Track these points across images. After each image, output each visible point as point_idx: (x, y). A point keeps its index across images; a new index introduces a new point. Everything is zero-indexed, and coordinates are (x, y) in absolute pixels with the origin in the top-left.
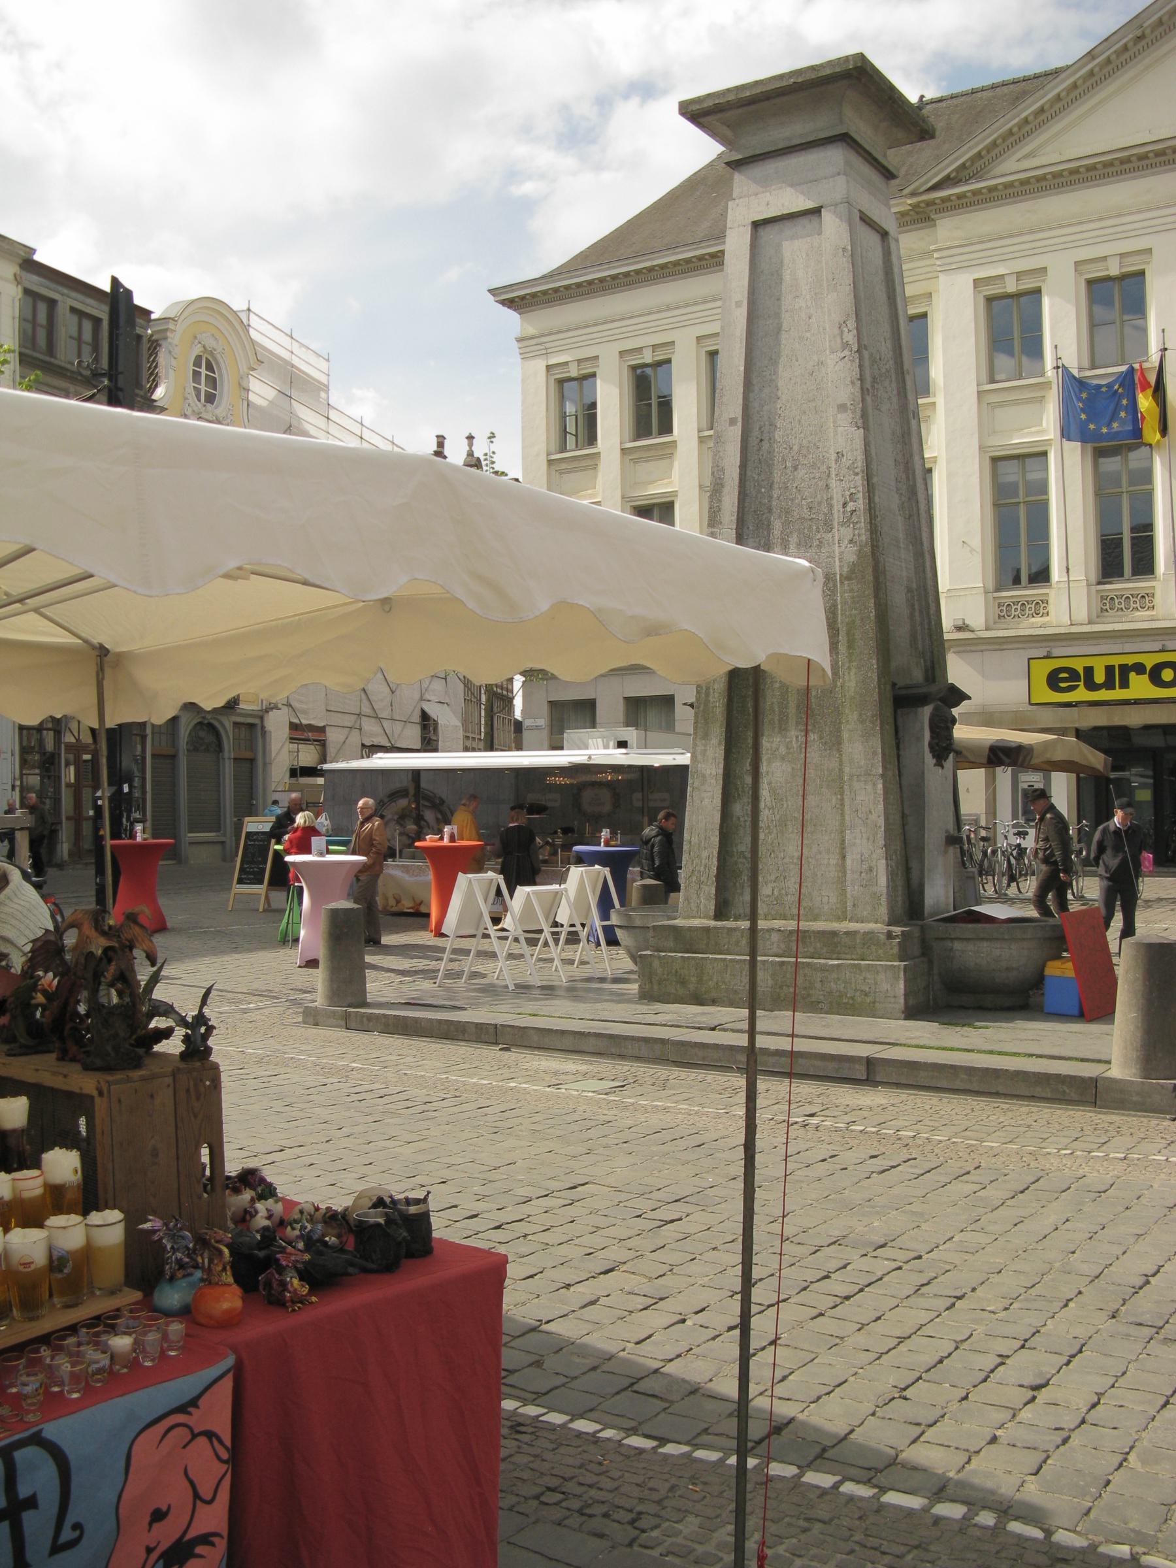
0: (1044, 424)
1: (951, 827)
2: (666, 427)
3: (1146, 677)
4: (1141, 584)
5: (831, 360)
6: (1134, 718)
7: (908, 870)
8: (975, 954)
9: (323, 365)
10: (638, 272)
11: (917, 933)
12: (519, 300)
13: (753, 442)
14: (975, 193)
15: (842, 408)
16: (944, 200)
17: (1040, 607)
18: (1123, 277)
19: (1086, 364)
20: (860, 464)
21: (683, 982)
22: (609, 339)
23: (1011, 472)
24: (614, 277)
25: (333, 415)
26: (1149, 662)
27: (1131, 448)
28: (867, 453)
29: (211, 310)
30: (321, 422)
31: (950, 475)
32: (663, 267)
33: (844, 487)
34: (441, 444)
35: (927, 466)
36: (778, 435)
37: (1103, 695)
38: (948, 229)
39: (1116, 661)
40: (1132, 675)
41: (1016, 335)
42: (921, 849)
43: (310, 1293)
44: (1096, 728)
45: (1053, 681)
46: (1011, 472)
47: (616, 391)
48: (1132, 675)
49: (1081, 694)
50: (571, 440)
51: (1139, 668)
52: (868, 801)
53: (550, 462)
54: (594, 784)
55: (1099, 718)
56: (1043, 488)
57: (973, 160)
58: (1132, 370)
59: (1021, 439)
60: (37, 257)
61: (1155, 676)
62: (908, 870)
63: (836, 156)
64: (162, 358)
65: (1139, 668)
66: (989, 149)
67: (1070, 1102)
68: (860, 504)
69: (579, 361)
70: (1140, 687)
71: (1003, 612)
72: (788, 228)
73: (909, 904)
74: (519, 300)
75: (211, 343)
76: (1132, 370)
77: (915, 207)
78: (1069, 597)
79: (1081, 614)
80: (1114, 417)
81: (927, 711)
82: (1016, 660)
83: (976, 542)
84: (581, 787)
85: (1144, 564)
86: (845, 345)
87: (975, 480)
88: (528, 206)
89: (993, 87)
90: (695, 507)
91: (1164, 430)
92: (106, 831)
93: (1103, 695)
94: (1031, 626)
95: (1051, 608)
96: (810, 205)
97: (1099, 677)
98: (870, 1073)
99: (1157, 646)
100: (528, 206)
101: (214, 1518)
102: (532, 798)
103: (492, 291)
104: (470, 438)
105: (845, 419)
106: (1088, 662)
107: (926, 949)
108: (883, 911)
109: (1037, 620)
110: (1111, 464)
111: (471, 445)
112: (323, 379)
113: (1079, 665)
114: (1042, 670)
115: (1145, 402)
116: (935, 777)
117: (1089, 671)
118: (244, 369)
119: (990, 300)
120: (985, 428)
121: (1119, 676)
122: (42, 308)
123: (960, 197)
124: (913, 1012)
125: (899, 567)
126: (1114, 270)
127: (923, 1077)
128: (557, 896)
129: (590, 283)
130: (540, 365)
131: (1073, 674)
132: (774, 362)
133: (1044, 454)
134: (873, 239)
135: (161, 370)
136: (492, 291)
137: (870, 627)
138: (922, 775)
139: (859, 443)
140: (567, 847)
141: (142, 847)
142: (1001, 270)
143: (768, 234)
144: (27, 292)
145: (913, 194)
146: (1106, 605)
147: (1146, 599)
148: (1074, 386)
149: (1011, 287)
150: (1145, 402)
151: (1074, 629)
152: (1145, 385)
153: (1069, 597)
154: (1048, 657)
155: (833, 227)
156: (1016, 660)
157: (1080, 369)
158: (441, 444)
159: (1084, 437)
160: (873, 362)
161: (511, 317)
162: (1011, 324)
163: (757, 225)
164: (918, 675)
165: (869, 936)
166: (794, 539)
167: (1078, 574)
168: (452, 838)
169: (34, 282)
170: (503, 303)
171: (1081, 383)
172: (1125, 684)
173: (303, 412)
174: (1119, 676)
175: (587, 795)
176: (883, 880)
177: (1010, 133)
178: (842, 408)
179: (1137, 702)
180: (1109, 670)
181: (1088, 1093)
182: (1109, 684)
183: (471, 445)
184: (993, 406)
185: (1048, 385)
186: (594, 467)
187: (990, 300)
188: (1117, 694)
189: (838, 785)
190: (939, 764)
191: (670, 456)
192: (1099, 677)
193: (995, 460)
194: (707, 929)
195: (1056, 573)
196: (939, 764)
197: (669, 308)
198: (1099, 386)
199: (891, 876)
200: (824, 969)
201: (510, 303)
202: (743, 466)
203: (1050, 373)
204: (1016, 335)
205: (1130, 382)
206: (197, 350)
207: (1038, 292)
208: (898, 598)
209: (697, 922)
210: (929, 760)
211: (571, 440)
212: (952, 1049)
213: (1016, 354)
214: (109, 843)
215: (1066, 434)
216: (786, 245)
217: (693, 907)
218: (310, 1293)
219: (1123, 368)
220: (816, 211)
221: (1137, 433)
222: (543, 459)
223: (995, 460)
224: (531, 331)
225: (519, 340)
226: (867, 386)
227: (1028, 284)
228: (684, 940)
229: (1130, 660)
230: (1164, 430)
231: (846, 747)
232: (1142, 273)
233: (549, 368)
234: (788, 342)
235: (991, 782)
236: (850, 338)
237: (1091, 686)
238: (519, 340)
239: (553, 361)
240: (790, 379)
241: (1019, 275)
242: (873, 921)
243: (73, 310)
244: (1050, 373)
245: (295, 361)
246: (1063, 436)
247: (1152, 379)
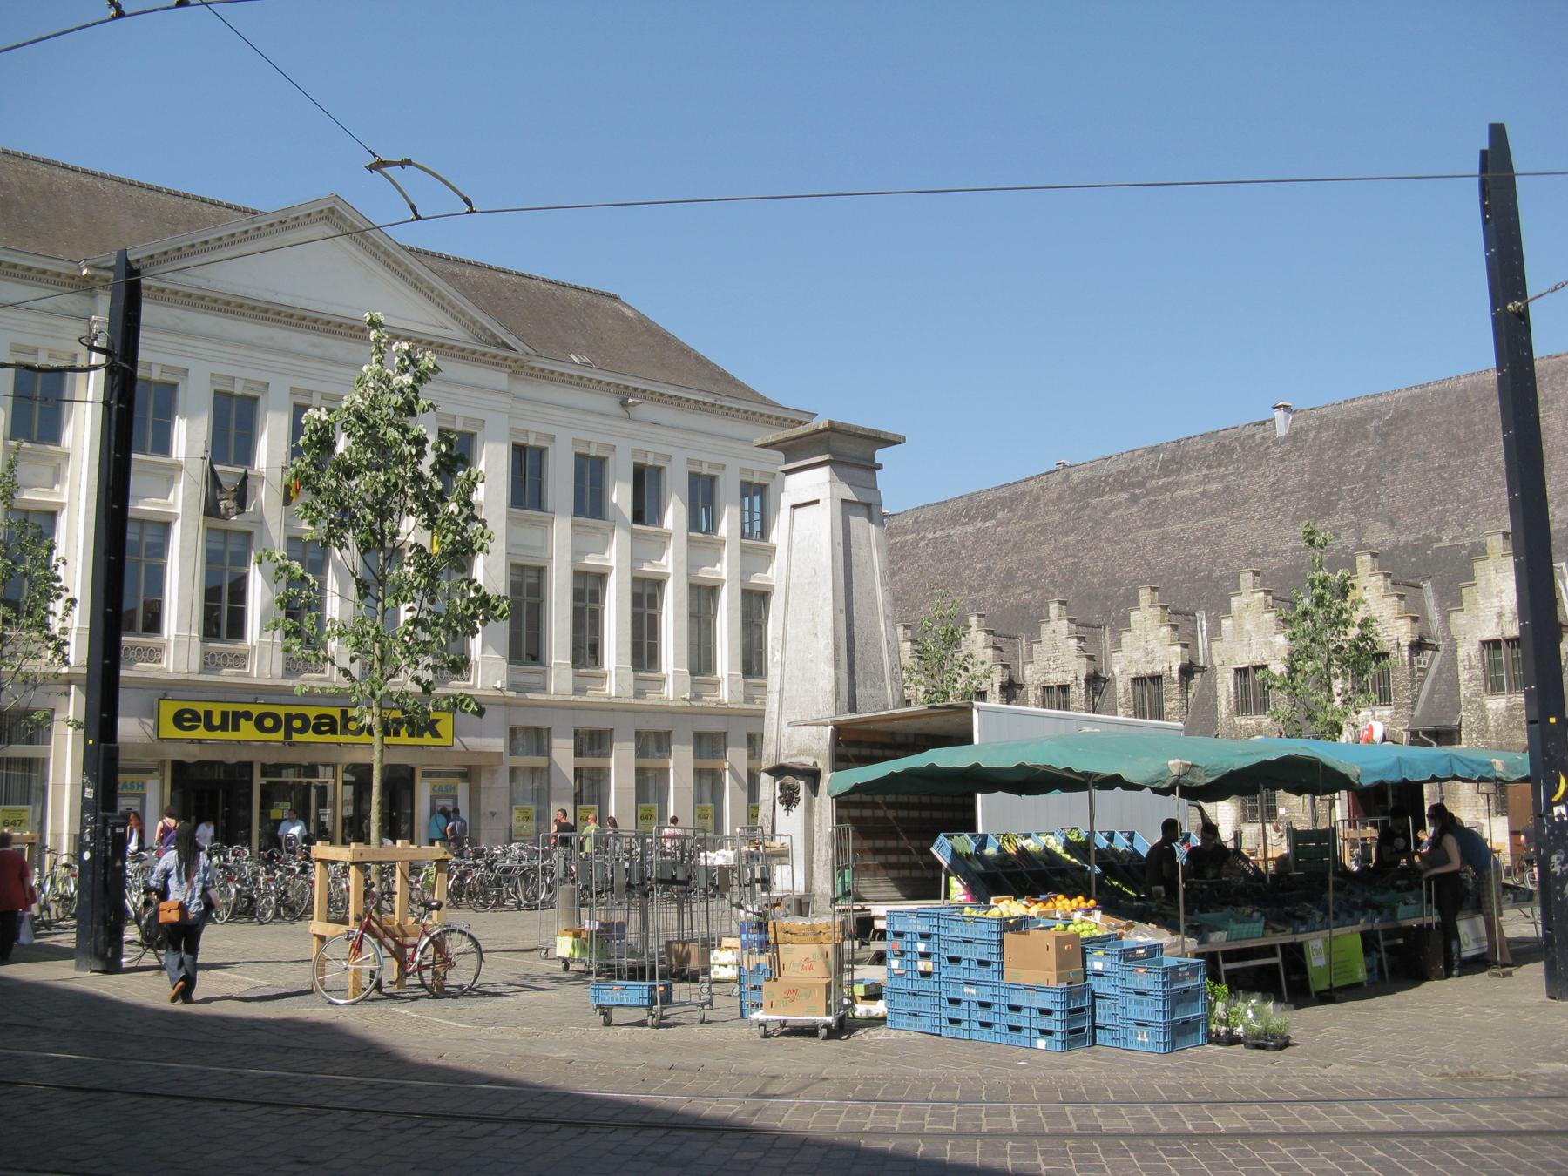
3: (252, 723)
18: (242, 398)
26: (256, 710)
39: (230, 708)
40: (242, 721)
43: (203, 849)
45: (179, 719)
48: (242, 721)
49: (201, 733)
61: (260, 726)
70: (247, 731)
97: (216, 720)
106: (208, 706)
113: (200, 708)
114: (169, 710)
117: (208, 714)
126: (238, 390)
131: (195, 716)
146: (211, 662)
172: (236, 728)
174: (231, 721)
180: (225, 715)
182: (223, 727)
185: (178, 467)
188: (229, 735)
192: (216, 720)
212: (713, 435)
213: (374, 834)
218: (203, 849)
229: (241, 708)
235: (125, 795)
237: (210, 727)
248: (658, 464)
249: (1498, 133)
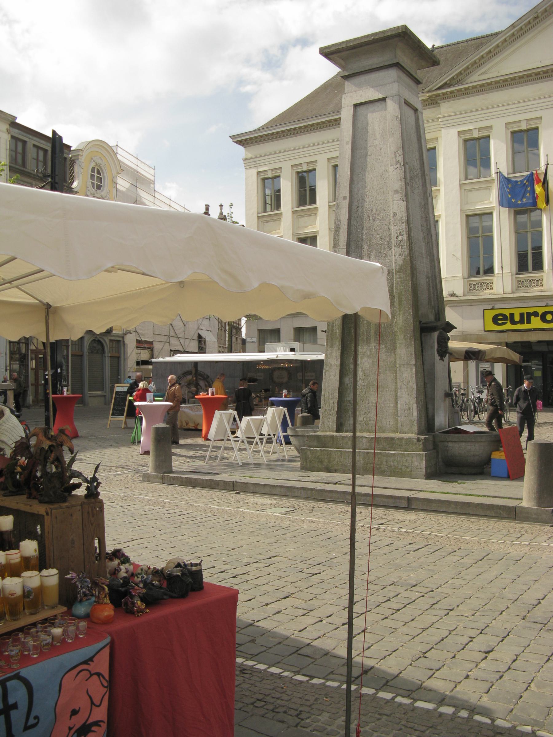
0: (491, 199)
1: (447, 389)
2: (313, 201)
3: (539, 318)
4: (537, 275)
5: (391, 169)
6: (533, 338)
7: (427, 409)
8: (459, 449)
9: (152, 172)
10: (300, 128)
11: (431, 438)
12: (244, 141)
13: (354, 208)
14: (458, 91)
15: (396, 192)
16: (444, 94)
17: (489, 285)
18: (528, 130)
19: (511, 171)
20: (404, 218)
21: (321, 462)
22: (286, 159)
23: (475, 222)
24: (289, 130)
25: (156, 195)
26: (541, 311)
27: (532, 211)
28: (408, 213)
29: (99, 146)
30: (151, 198)
31: (447, 223)
32: (312, 125)
33: (397, 229)
34: (207, 209)
35: (436, 219)
36: (366, 204)
37: (519, 327)
38: (446, 108)
39: (525, 311)
40: (532, 317)
41: (478, 157)
42: (433, 399)
43: (146, 608)
44: (515, 342)
45: (495, 320)
46: (475, 222)
47: (290, 184)
48: (532, 317)
49: (509, 326)
50: (268, 207)
51: (536, 314)
52: (408, 376)
53: (259, 217)
54: (279, 369)
55: (517, 338)
56: (491, 229)
57: (457, 75)
58: (532, 174)
59: (480, 206)
60: (17, 121)
61: (543, 318)
62: (427, 409)
63: (393, 73)
64: (76, 168)
65: (536, 314)
66: (465, 70)
67: (503, 518)
68: (405, 237)
69: (272, 170)
70: (536, 323)
71: (472, 288)
72: (371, 107)
73: (428, 425)
74: (244, 141)
75: (99, 161)
76: (532, 174)
77: (430, 97)
78: (503, 280)
79: (508, 288)
80: (524, 196)
81: (436, 334)
82: (478, 310)
83: (459, 255)
84: (273, 370)
85: (538, 265)
86: (398, 162)
87: (459, 226)
88: (248, 97)
89: (467, 41)
90: (327, 239)
91: (547, 202)
92: (50, 391)
93: (519, 327)
94: (485, 294)
95: (494, 286)
96: (381, 96)
97: (517, 318)
98: (409, 504)
99: (544, 304)
100: (248, 97)
101: (101, 714)
102: (250, 375)
103: (231, 137)
104: (221, 206)
105: (397, 197)
106: (512, 311)
107: (435, 446)
108: (415, 428)
109: (488, 291)
110: (523, 218)
111: (221, 209)
112: (152, 178)
113: (507, 313)
114: (490, 315)
115: (538, 189)
116: (440, 365)
117: (512, 315)
118: (115, 173)
119: (465, 141)
120: (463, 201)
121: (526, 318)
122: (20, 145)
123: (451, 92)
124: (429, 476)
125: (423, 266)
126: (524, 127)
127: (434, 506)
128: (262, 421)
129: (278, 133)
130: (254, 172)
131: (505, 317)
132: (364, 170)
133: (491, 213)
134: (411, 112)
135: (76, 174)
136: (231, 137)
137: (409, 295)
138: (433, 364)
139: (404, 208)
140: (267, 398)
141: (67, 398)
142: (471, 127)
143: (361, 110)
144: (13, 137)
145: (430, 91)
146: (520, 284)
147: (539, 282)
148: (505, 181)
149: (475, 135)
150: (538, 189)
151: (505, 296)
152: (538, 181)
153: (503, 280)
154: (493, 309)
155: (392, 107)
156: (478, 310)
157: (508, 173)
158: (207, 209)
159: (510, 205)
160: (411, 170)
161: (240, 149)
162: (475, 152)
163: (356, 106)
164: (432, 317)
165: (409, 440)
166: (373, 253)
167: (507, 270)
168: (213, 394)
169: (16, 132)
170: (237, 142)
171: (508, 180)
172: (529, 322)
173: (142, 194)
174: (526, 318)
175: (276, 374)
176: (415, 414)
177: (475, 62)
178: (396, 192)
179: (535, 330)
180: (522, 315)
181: (512, 514)
182: (521, 322)
183: (221, 209)
184: (467, 191)
185: (493, 181)
186: (280, 220)
187: (465, 141)
188: (525, 326)
189: (394, 369)
190: (442, 359)
191: (315, 214)
192: (517, 318)
193: (468, 216)
194: (332, 437)
195: (497, 269)
196: (442, 359)
197: (315, 145)
198: (517, 182)
199: (419, 412)
200: (388, 455)
201: (240, 143)
202: (350, 219)
203: (494, 175)
204: (478, 157)
205: (531, 179)
206: (93, 165)
207: (488, 137)
208: (422, 281)
209: (328, 434)
210: (437, 357)
211: (268, 207)
214: (51, 396)
215: (501, 204)
216: (370, 115)
217: (326, 426)
218: (146, 608)
219: (528, 173)
220: (384, 99)
221: (535, 203)
222: (255, 216)
223: (468, 216)
224: (250, 155)
225: (244, 160)
226: (408, 181)
227: (483, 134)
228: (322, 442)
229: (531, 310)
230: (547, 202)
231: (398, 351)
232: (537, 129)
233: (258, 173)
234: (370, 161)
235: (466, 368)
236: (400, 159)
237: (513, 322)
238: (244, 160)
239: (260, 169)
240: (371, 178)
241: (479, 129)
242: (410, 433)
243: (34, 146)
244: (494, 175)
245: (139, 170)
246: (500, 205)
247: (542, 178)
248: (256, 333)
249: (70, 719)
